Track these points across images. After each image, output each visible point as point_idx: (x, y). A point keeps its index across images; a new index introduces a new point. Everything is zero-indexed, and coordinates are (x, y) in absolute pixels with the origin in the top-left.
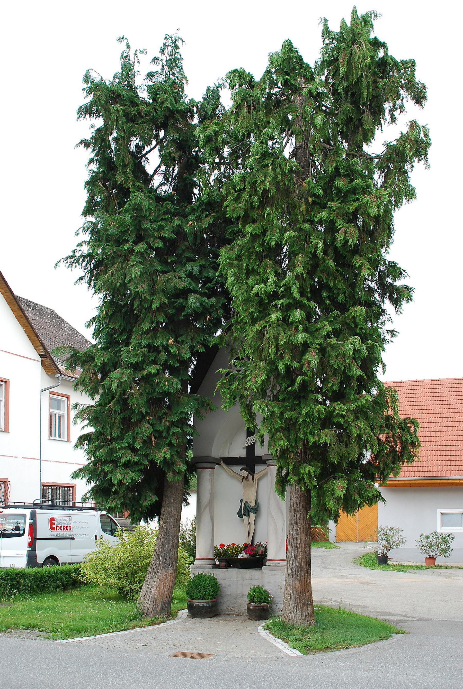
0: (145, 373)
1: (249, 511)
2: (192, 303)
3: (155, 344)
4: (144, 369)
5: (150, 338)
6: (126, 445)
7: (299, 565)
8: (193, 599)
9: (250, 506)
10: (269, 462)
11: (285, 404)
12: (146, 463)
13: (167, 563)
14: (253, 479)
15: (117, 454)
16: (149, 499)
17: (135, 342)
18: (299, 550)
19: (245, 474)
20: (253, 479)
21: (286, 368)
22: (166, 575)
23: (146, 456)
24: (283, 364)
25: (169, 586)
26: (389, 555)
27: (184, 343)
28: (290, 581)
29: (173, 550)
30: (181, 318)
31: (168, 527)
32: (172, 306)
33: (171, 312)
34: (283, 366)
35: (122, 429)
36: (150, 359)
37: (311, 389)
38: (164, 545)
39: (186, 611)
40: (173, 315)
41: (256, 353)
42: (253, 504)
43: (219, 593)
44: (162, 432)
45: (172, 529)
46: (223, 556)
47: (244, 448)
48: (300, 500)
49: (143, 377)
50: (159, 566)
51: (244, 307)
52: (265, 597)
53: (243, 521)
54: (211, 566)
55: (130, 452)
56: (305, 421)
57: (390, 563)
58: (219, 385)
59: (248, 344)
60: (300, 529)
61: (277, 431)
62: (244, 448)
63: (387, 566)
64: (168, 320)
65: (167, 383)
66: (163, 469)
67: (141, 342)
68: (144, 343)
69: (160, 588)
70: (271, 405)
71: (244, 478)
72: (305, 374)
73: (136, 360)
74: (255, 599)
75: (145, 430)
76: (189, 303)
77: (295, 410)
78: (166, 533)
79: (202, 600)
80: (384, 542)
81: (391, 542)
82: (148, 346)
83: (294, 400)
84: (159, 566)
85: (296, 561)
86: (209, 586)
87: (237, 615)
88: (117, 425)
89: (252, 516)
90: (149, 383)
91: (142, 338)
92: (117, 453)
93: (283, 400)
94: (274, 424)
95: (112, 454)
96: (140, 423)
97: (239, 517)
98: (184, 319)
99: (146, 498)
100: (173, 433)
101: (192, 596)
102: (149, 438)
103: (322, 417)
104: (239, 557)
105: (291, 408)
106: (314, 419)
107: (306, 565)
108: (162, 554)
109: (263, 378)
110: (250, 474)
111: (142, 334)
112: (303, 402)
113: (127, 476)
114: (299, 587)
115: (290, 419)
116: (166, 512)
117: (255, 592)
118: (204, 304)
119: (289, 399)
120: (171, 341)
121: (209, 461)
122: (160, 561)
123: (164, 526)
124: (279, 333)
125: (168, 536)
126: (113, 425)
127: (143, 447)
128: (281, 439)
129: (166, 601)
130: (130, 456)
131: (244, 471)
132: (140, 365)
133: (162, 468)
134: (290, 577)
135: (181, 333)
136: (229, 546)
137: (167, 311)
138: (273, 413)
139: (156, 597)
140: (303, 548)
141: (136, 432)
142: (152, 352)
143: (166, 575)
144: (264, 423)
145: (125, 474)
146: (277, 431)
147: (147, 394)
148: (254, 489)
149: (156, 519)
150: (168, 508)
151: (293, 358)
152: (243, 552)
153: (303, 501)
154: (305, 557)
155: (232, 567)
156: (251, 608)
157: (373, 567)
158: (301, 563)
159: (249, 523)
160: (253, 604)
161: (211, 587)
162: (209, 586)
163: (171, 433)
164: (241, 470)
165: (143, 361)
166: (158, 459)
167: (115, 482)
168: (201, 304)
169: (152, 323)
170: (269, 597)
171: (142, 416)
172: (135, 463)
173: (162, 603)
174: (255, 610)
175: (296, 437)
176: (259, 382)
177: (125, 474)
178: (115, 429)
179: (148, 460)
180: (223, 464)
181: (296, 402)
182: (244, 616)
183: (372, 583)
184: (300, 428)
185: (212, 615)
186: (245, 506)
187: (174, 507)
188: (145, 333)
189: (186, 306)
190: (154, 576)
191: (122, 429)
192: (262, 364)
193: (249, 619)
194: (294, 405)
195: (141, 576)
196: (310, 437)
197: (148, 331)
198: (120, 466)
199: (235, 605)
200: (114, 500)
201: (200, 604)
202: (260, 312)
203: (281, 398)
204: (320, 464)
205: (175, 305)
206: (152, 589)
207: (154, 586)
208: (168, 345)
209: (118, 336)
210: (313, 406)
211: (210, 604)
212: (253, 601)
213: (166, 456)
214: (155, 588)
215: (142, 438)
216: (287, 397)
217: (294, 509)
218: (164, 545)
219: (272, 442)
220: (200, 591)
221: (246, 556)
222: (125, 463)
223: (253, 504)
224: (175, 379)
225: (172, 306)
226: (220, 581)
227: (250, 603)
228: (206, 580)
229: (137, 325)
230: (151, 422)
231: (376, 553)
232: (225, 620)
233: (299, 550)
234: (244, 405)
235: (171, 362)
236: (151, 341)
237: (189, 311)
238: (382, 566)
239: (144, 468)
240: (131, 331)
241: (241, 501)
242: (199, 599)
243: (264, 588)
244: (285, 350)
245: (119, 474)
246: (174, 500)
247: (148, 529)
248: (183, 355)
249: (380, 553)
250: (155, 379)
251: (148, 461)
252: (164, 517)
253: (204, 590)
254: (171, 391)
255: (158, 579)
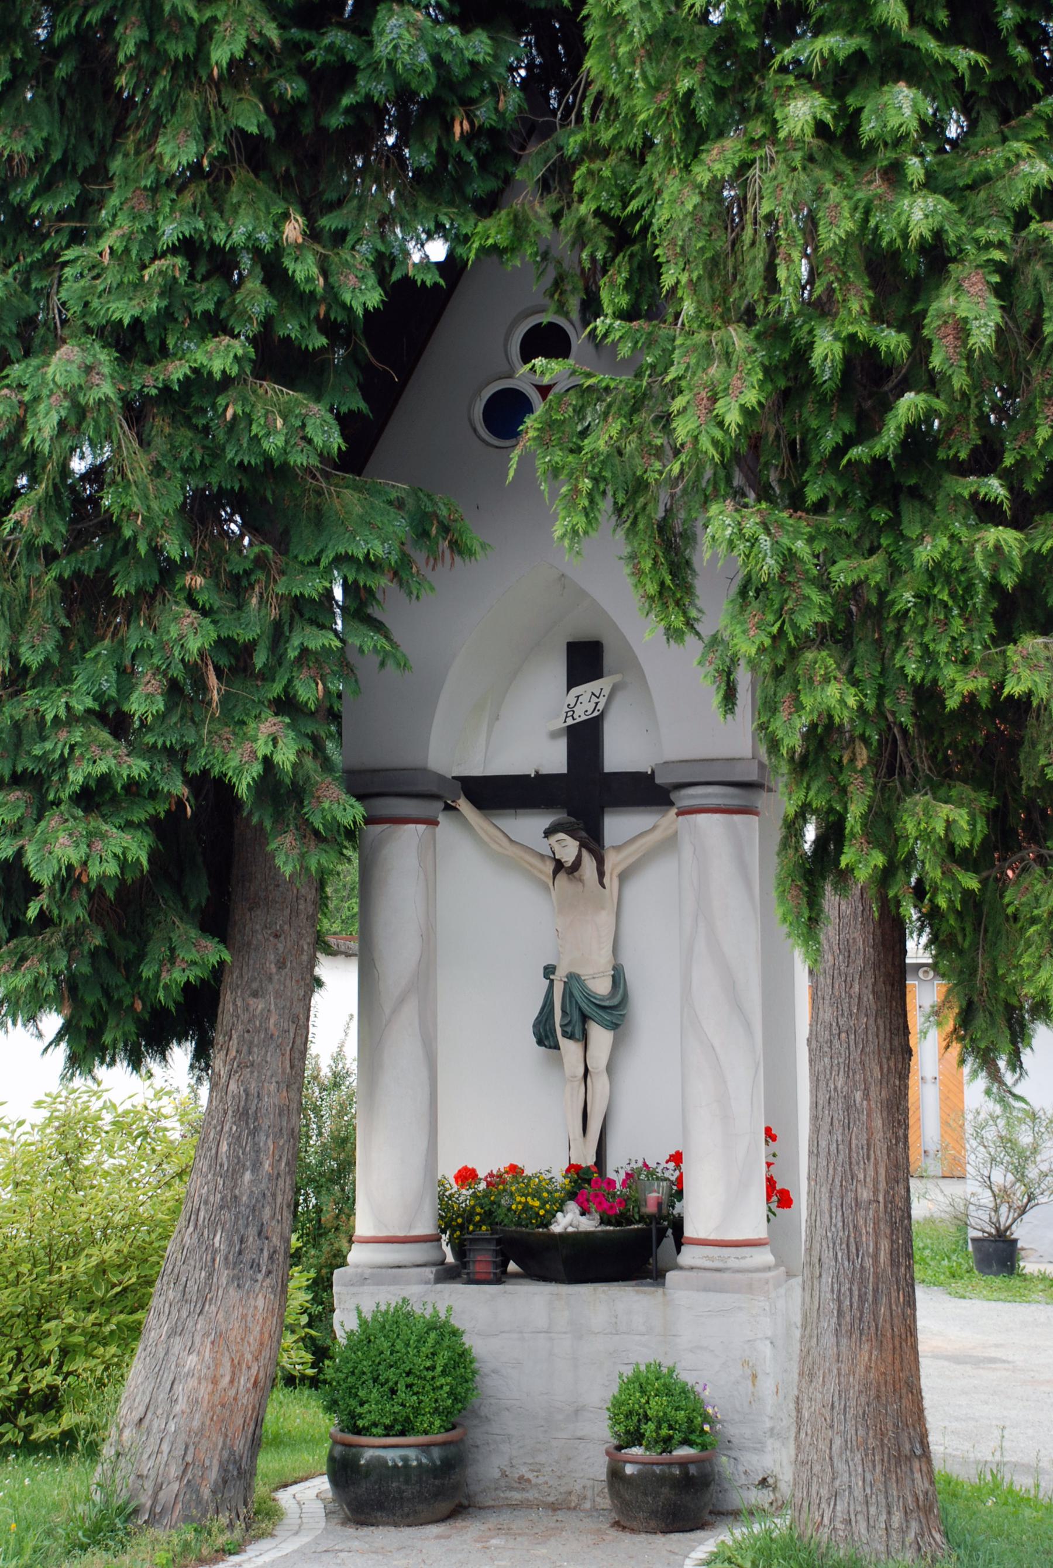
0: (177, 371)
1: (585, 1018)
2: (396, 47)
3: (219, 237)
4: (164, 352)
5: (196, 210)
6: (89, 703)
7: (868, 1263)
8: (358, 1431)
9: (589, 996)
10: (687, 797)
11: (831, 521)
12: (179, 788)
13: (247, 1257)
14: (601, 874)
15: (48, 746)
16: (189, 957)
17: (124, 223)
18: (865, 1195)
19: (568, 848)
20: (601, 874)
21: (847, 359)
22: (244, 1317)
23: (178, 755)
24: (836, 337)
25: (254, 1371)
26: (1020, 1233)
27: (351, 239)
28: (829, 1340)
29: (274, 1195)
30: (336, 121)
31: (253, 1090)
32: (291, 64)
33: (292, 88)
34: (838, 348)
35: (63, 630)
36: (199, 308)
37: (956, 456)
38: (233, 1174)
39: (323, 1484)
40: (298, 105)
41: (705, 284)
42: (601, 987)
43: (473, 1400)
44: (250, 648)
45: (272, 1097)
46: (478, 1225)
47: (554, 735)
48: (860, 962)
49: (166, 390)
50: (210, 1275)
51: (650, 73)
52: (690, 1420)
53: (559, 1062)
54: (429, 1273)
55: (105, 736)
56: (925, 600)
57: (1028, 1266)
58: (532, 434)
59: (673, 242)
60: (866, 1096)
61: (806, 642)
62: (554, 735)
63: (1015, 1282)
64: (276, 126)
65: (279, 423)
66: (255, 820)
67: (153, 230)
68: (170, 231)
69: (215, 1382)
70: (781, 525)
71: (559, 865)
72: (932, 383)
73: (136, 312)
74: (649, 1428)
75: (181, 637)
76: (382, 48)
77: (872, 551)
78: (243, 1115)
79: (402, 1433)
80: (1000, 1177)
81: (1032, 1173)
82: (187, 247)
83: (869, 505)
84: (210, 1275)
85: (852, 1247)
86: (433, 1368)
87: (554, 1508)
88: (42, 611)
89: (600, 1037)
90: (188, 418)
91: (156, 210)
92: (43, 739)
93: (820, 507)
94: (792, 611)
95: (18, 744)
96: (150, 607)
97: (540, 1042)
98: (347, 128)
99: (172, 950)
100: (304, 651)
101: (353, 1416)
102: (195, 672)
103: (1008, 580)
104: (556, 1228)
105: (857, 543)
106: (969, 588)
107: (894, 1263)
108: (226, 1215)
109: (751, 397)
110: (591, 851)
111: (155, 190)
112: (910, 514)
113: (99, 845)
114: (868, 1369)
115: (857, 588)
116: (245, 1017)
117: (643, 1392)
118: (447, 57)
119: (843, 502)
120: (293, 230)
121: (405, 789)
122: (215, 1252)
123: (233, 1086)
124: (820, 194)
125: (254, 1132)
126: (25, 611)
127: (161, 717)
128: (827, 680)
129: (240, 1445)
130: (109, 754)
131: (561, 836)
132: (149, 337)
133: (250, 814)
134: (828, 1323)
135: (331, 196)
136: (495, 1180)
137: (270, 83)
138: (789, 558)
139: (196, 1424)
140: (882, 1186)
141: (132, 645)
142: (204, 279)
143: (244, 1317)
144: (743, 608)
145: (92, 837)
146: (806, 642)
147: (185, 471)
148: (606, 918)
149: (181, 1054)
150: (252, 1001)
151: (877, 315)
152: (572, 1208)
153: (876, 966)
154: (893, 1224)
155: (515, 1276)
156: (629, 1469)
157: (958, 1286)
158: (876, 1256)
159: (586, 1071)
160: (636, 1451)
161: (444, 1373)
162: (433, 1368)
163: (292, 654)
164: (548, 833)
165: (167, 316)
166: (239, 771)
167: (43, 875)
168: (436, 60)
169: (207, 135)
170: (707, 1418)
171: (162, 572)
172: (133, 787)
173: (225, 1454)
174: (647, 1481)
175: (883, 673)
176: (733, 418)
177: (92, 837)
178: (31, 628)
179: (185, 774)
180: (464, 805)
181: (881, 515)
182: (589, 1513)
183: (992, 1360)
184: (900, 629)
185: (445, 1507)
186: (568, 994)
187: (278, 995)
188: (168, 184)
189: (362, 64)
190: (190, 1324)
191: (63, 630)
192: (739, 338)
193: (617, 1524)
194: (869, 526)
195: (71, 1329)
196: (950, 672)
197: (177, 184)
198: (57, 803)
199: (542, 1458)
200: (23, 958)
201: (392, 1456)
202: (720, 94)
203: (813, 495)
204: (984, 800)
205: (310, 55)
206: (179, 1388)
207: (190, 1374)
208: (278, 249)
209: (34, 196)
210: (964, 534)
211: (436, 1452)
212: (635, 1438)
213: (278, 758)
214: (192, 1383)
215: (165, 674)
216: (839, 491)
217: (837, 1003)
218: (233, 1174)
219: (784, 694)
220: (393, 1392)
221: (588, 1224)
222: (85, 789)
223: (601, 987)
224: (315, 408)
225: (291, 64)
226: (475, 1343)
227: (619, 1448)
228: (421, 1340)
229: (130, 147)
230: (201, 599)
231: (962, 1223)
232: (509, 1532)
233: (865, 1195)
234: (648, 526)
235: (290, 328)
236: (201, 225)
237: (379, 89)
238: (998, 1281)
239: (168, 812)
240: (99, 173)
241: (549, 971)
242: (388, 1431)
243: (686, 1377)
244: (845, 274)
245: (63, 838)
246: (281, 965)
247: (96, 1105)
248: (347, 297)
249: (980, 1225)
250: (221, 401)
251: (189, 780)
252: (234, 1043)
253: (409, 1386)
254: (299, 459)
255: (206, 1335)
